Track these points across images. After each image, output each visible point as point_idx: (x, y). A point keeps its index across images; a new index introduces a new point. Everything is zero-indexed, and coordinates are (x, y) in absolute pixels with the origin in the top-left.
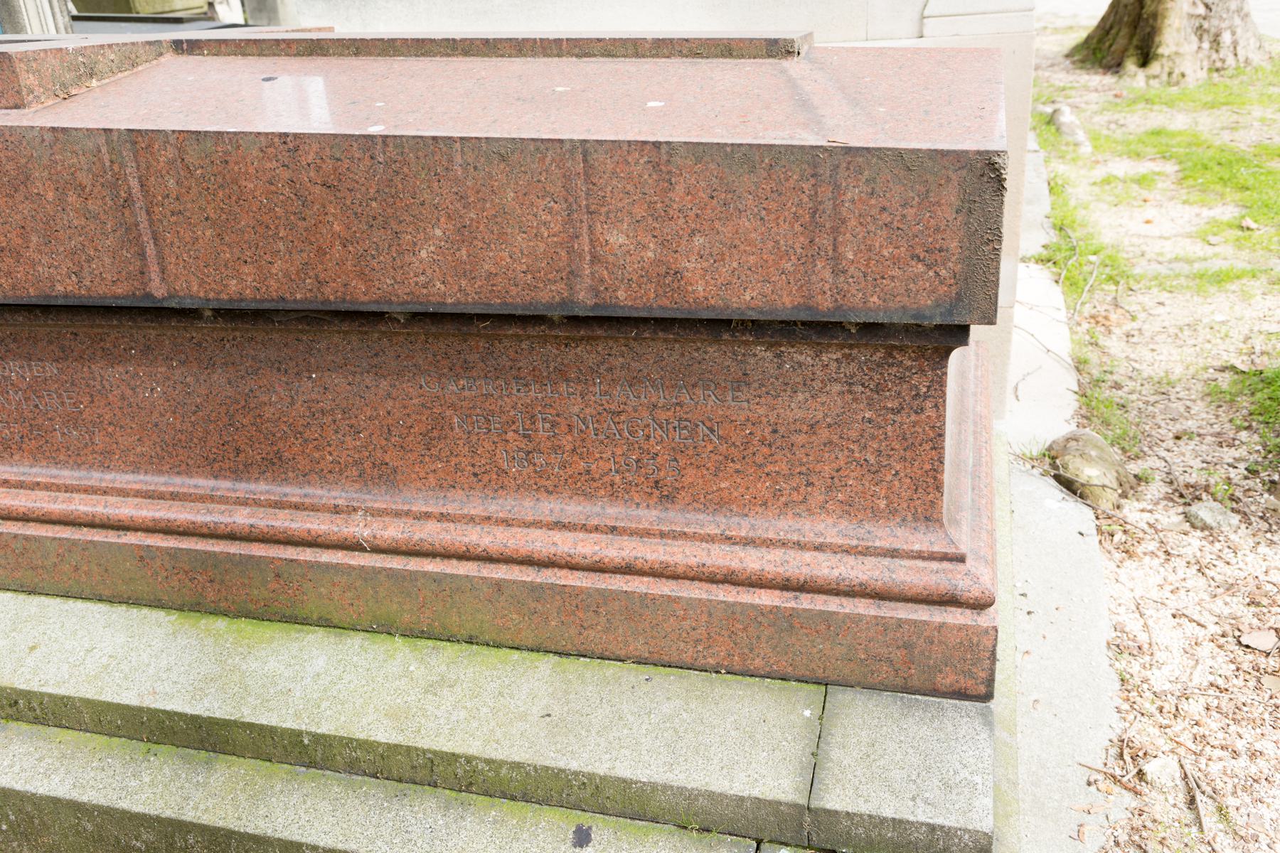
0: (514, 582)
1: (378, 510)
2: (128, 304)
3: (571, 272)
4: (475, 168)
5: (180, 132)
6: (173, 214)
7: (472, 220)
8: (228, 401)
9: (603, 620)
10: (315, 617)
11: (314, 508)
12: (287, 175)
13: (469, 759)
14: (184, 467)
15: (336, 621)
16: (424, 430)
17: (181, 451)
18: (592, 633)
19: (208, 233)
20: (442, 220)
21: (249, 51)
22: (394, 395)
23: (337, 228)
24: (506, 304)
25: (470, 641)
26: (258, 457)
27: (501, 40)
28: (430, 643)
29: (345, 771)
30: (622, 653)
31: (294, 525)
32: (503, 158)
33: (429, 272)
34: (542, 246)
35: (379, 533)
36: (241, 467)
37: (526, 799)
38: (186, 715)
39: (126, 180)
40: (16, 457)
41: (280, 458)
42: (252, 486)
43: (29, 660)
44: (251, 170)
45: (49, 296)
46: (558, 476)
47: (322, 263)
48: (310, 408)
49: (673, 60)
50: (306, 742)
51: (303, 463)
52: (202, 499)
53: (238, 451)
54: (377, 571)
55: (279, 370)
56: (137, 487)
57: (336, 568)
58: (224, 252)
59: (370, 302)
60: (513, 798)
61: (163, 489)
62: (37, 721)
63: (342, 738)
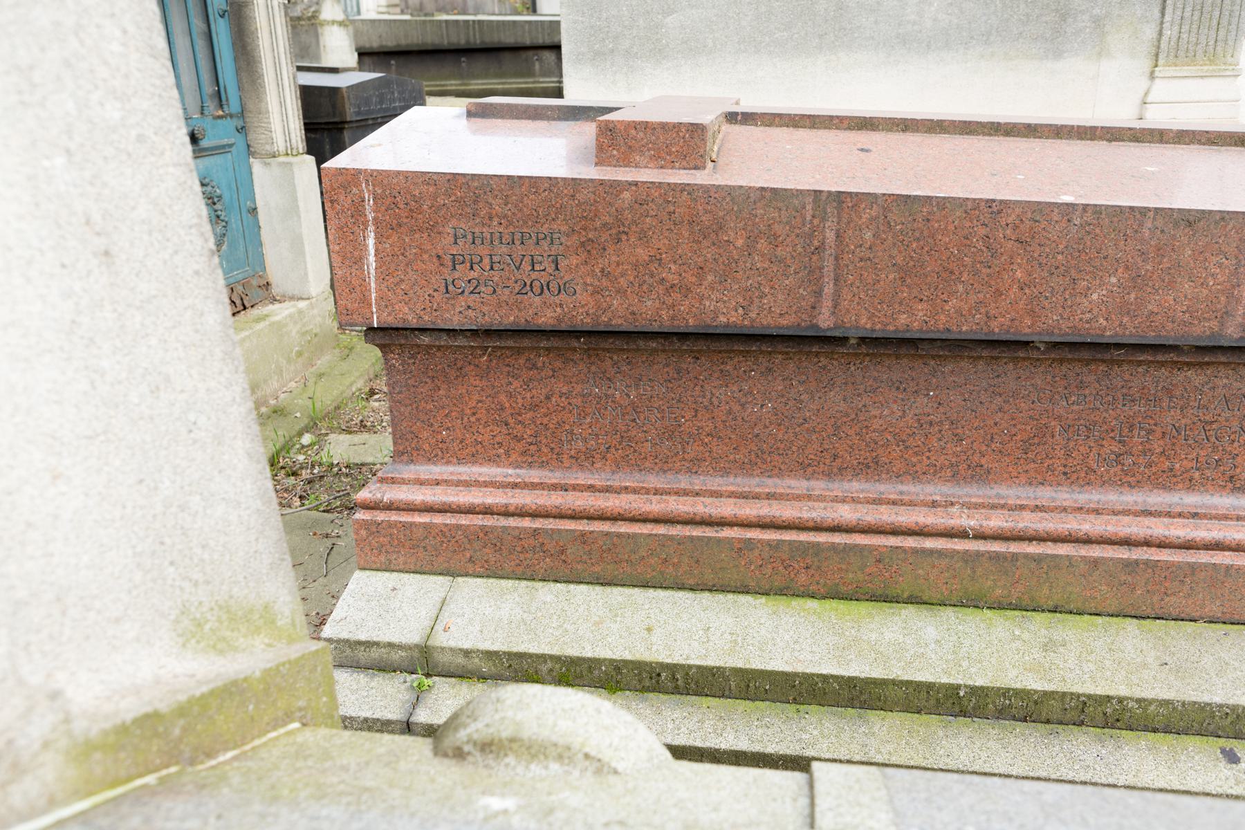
0: (1112, 559)
1: (976, 504)
2: (790, 333)
3: (1226, 313)
4: (1162, 231)
5: (890, 195)
6: (861, 260)
7: (1147, 271)
8: (838, 415)
9: (1186, 588)
10: (905, 596)
11: (912, 504)
12: (983, 231)
13: (1121, 700)
14: (777, 471)
15: (925, 599)
16: (1025, 437)
17: (776, 457)
18: (1173, 599)
19: (891, 277)
20: (1120, 270)
21: (801, 123)
22: (1006, 409)
23: (1019, 274)
24: (1160, 336)
25: (1054, 611)
26: (855, 462)
27: (1041, 125)
28: (1017, 613)
29: (993, 717)
30: (1195, 615)
31: (900, 519)
32: (1190, 224)
33: (1095, 311)
34: (1205, 292)
35: (985, 523)
36: (835, 470)
37: (1167, 731)
38: (843, 677)
39: (823, 231)
40: (598, 465)
41: (877, 463)
42: (846, 485)
43: (654, 639)
44: (951, 227)
45: (709, 326)
46: (1143, 473)
47: (996, 302)
48: (919, 420)
49: (1192, 146)
50: (962, 694)
51: (898, 466)
52: (798, 498)
53: (835, 457)
54: (979, 554)
55: (898, 388)
56: (732, 488)
57: (940, 553)
58: (903, 292)
59: (1032, 334)
60: (1155, 731)
61: (757, 490)
62: (676, 691)
63: (999, 689)
